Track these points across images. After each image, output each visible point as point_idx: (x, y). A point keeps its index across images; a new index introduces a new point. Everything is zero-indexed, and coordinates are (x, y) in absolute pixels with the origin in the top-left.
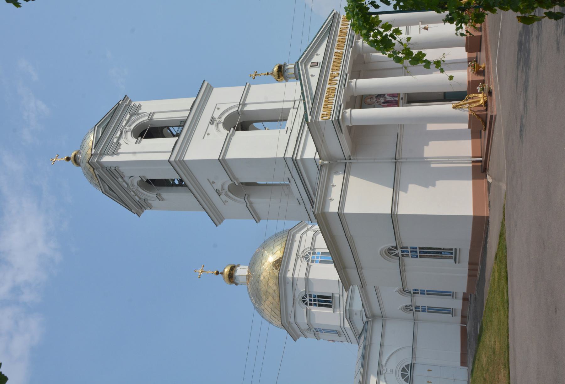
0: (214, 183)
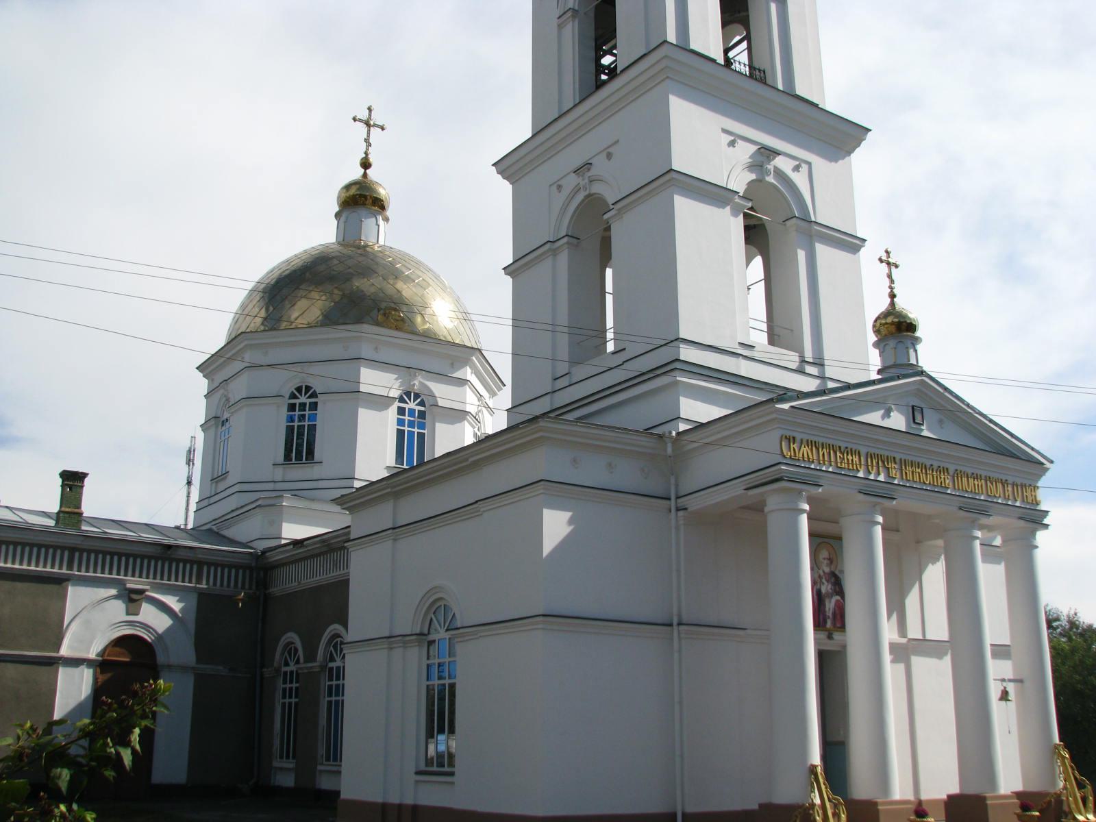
0: (609, 156)
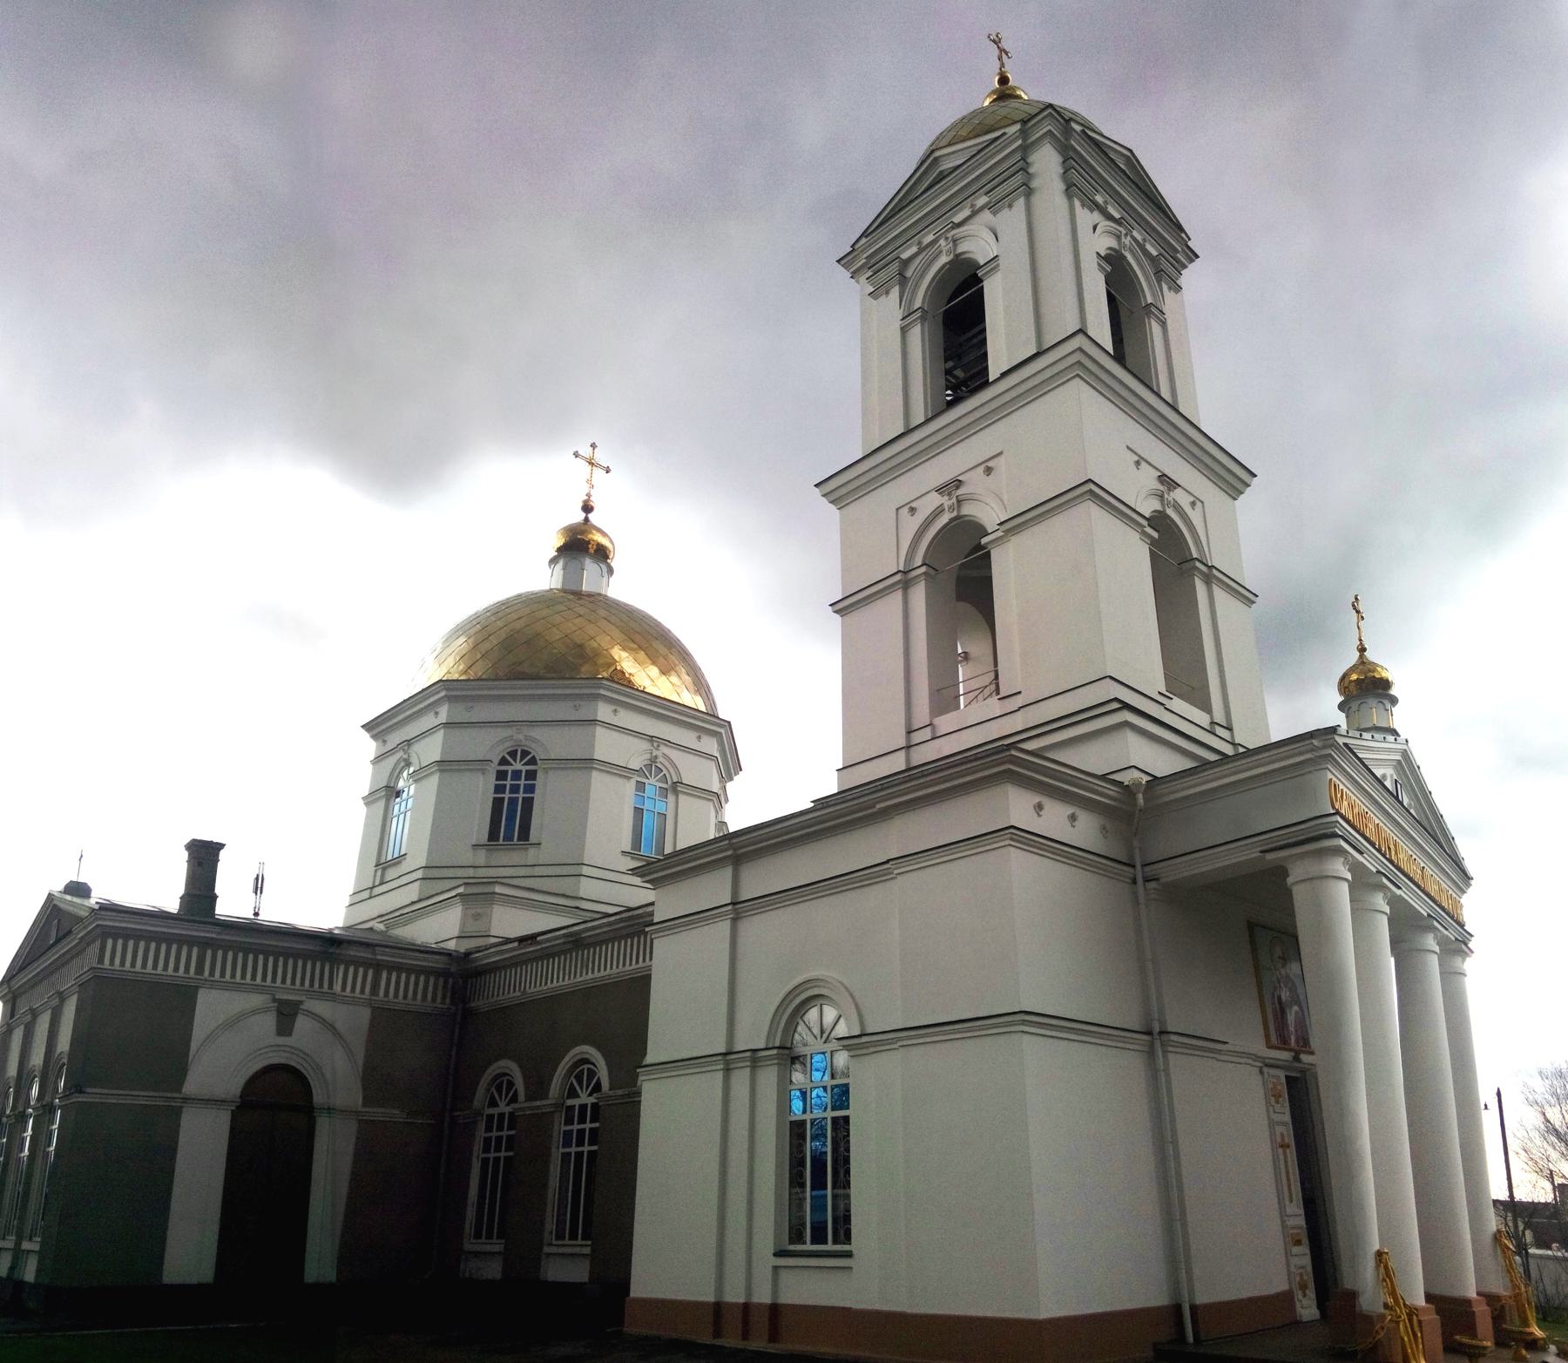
0: (989, 471)
